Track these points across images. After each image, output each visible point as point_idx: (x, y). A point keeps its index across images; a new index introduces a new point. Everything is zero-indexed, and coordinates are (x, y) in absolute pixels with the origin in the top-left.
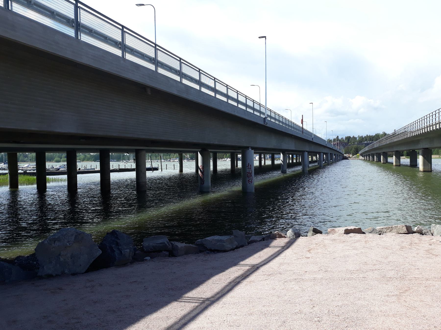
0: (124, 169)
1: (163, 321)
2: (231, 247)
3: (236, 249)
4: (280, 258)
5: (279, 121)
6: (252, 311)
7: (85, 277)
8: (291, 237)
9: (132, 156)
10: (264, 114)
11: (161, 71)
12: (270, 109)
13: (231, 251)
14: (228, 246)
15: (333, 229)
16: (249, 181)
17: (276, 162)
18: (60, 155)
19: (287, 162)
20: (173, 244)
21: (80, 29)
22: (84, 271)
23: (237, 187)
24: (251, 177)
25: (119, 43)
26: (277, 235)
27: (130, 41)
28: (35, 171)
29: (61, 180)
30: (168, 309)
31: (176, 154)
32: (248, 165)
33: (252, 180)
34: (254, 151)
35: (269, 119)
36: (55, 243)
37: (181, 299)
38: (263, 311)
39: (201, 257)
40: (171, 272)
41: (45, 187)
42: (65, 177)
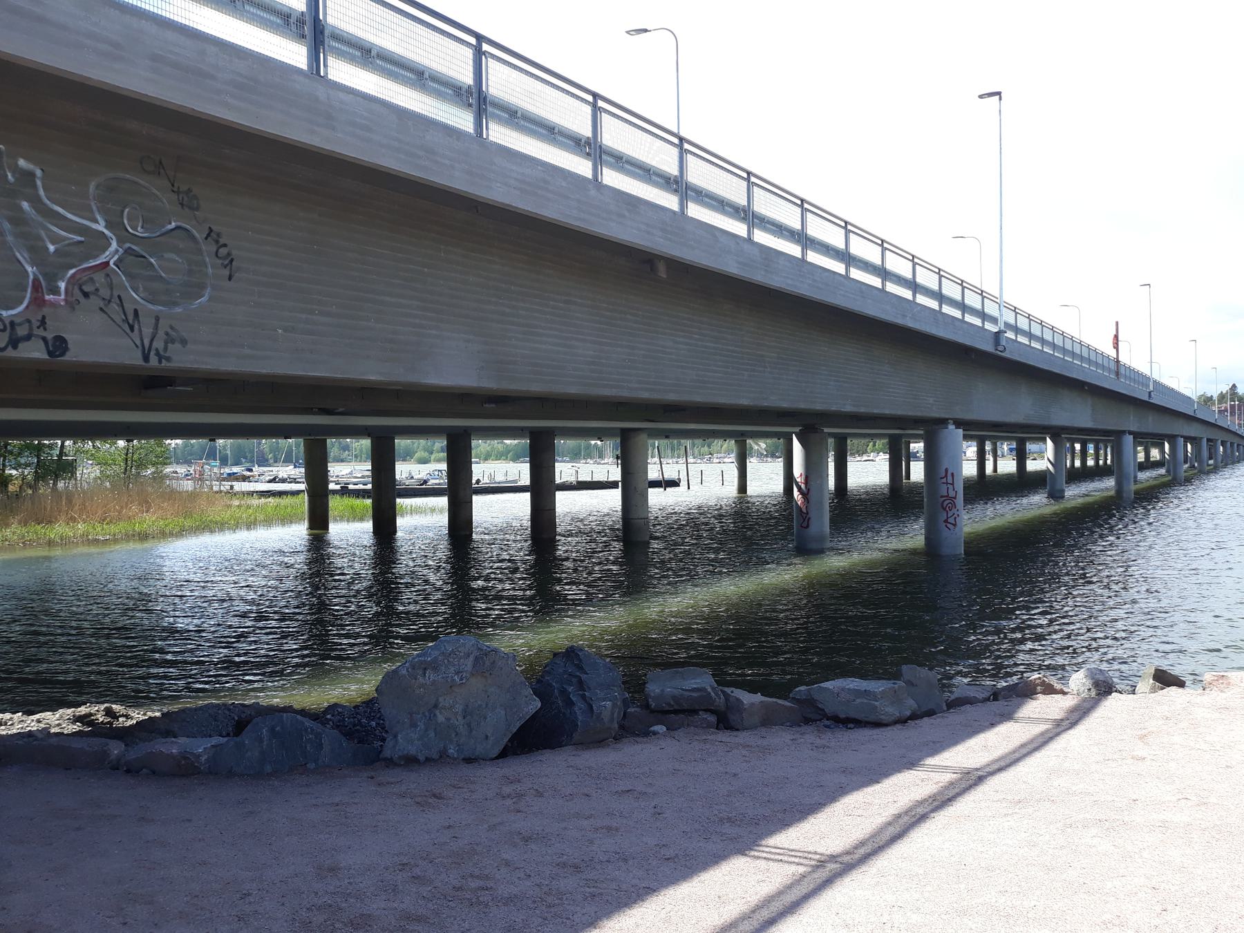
0: (589, 482)
1: (709, 906)
2: (898, 715)
3: (911, 719)
4: (1048, 753)
5: (1042, 341)
6: (965, 903)
7: (498, 769)
8: (1084, 691)
9: (609, 446)
10: (994, 320)
11: (695, 211)
12: (1029, 313)
13: (897, 725)
14: (889, 710)
15: (1223, 676)
16: (946, 521)
17: (1032, 466)
18: (429, 444)
19: (1066, 465)
20: (728, 694)
21: (485, 110)
22: (496, 751)
23: (913, 536)
24: (954, 511)
25: (586, 142)
26: (1038, 685)
27: (615, 135)
28: (369, 486)
29: (433, 510)
30: (721, 874)
32: (944, 475)
33: (955, 518)
35: (1010, 335)
36: (425, 674)
37: (756, 850)
38: (1002, 907)
39: (810, 736)
40: (726, 773)
41: (393, 529)
42: (443, 501)
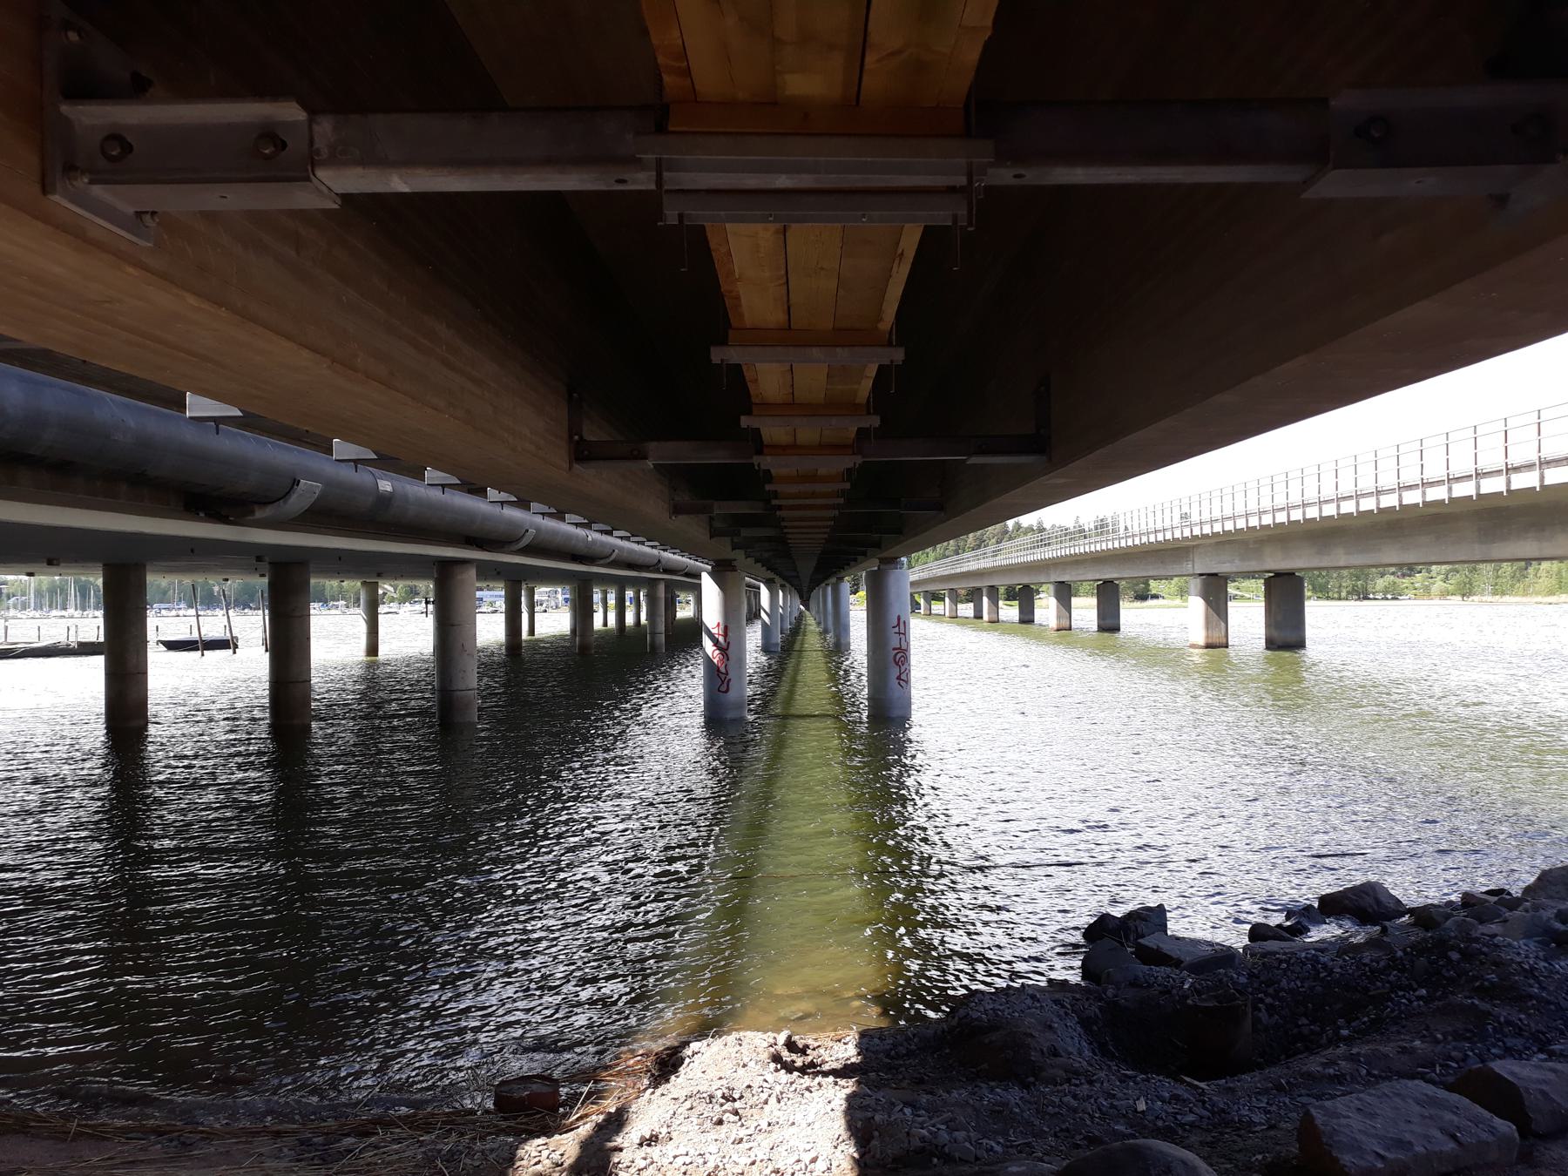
0: (93, 643)
34: (697, 581)
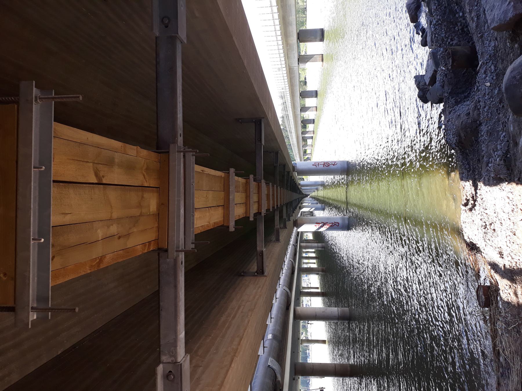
16: (334, 165)
31: (518, 117)
32: (315, 166)
34: (300, 233)
